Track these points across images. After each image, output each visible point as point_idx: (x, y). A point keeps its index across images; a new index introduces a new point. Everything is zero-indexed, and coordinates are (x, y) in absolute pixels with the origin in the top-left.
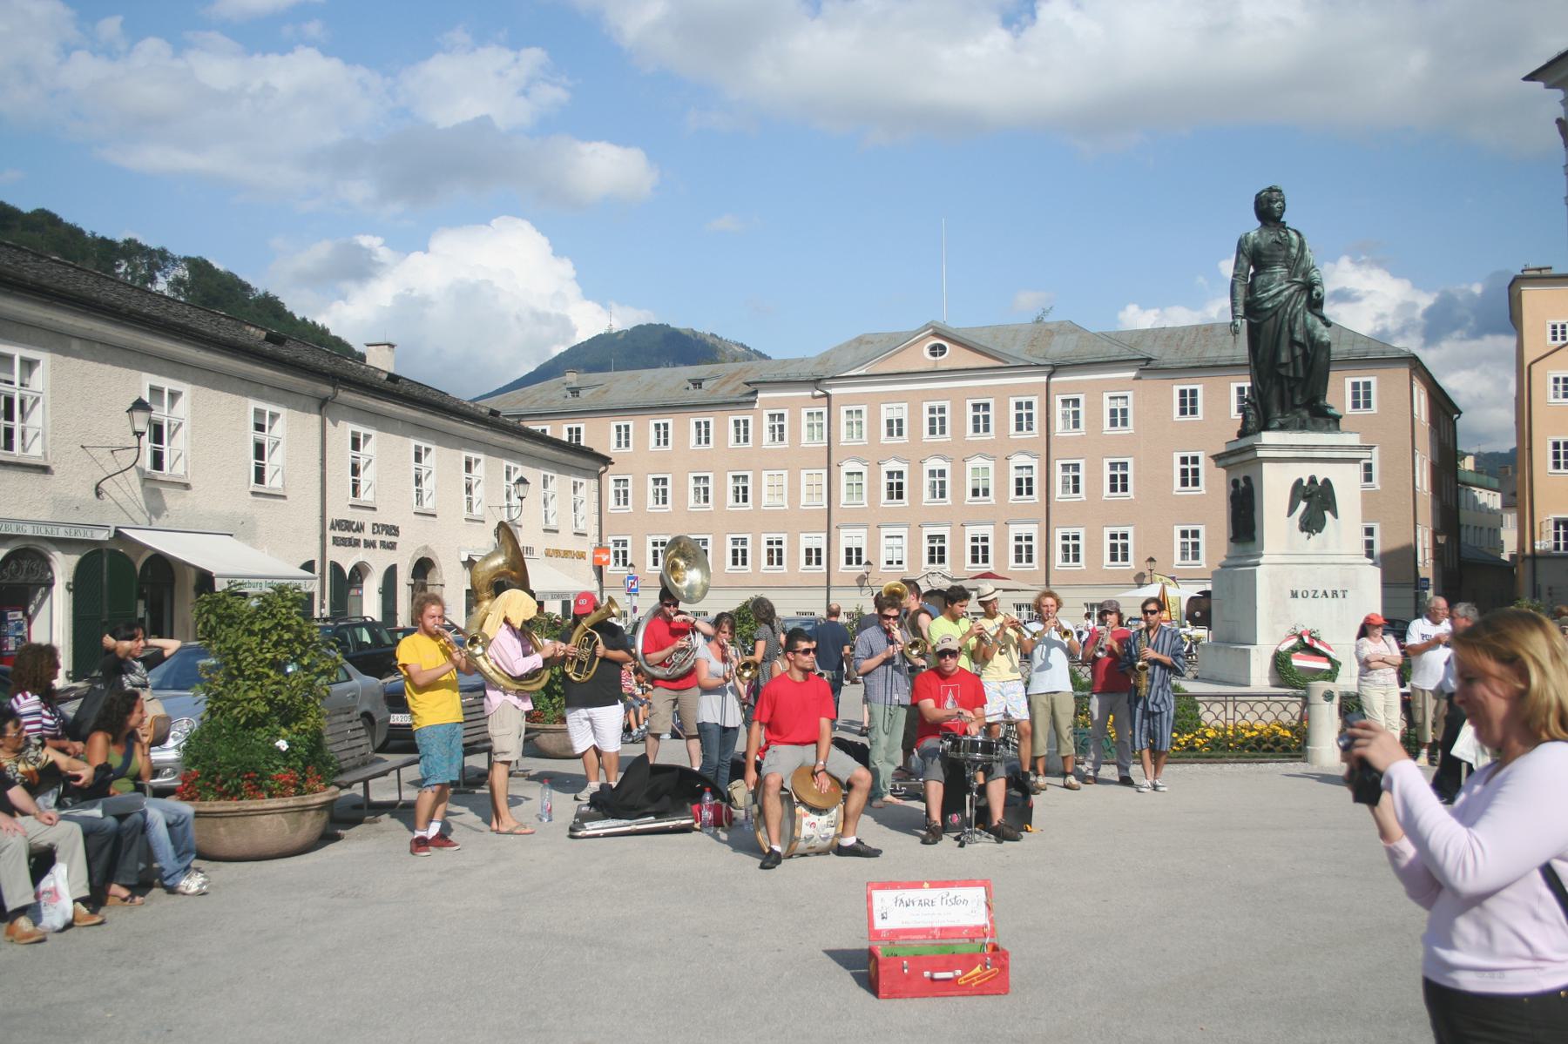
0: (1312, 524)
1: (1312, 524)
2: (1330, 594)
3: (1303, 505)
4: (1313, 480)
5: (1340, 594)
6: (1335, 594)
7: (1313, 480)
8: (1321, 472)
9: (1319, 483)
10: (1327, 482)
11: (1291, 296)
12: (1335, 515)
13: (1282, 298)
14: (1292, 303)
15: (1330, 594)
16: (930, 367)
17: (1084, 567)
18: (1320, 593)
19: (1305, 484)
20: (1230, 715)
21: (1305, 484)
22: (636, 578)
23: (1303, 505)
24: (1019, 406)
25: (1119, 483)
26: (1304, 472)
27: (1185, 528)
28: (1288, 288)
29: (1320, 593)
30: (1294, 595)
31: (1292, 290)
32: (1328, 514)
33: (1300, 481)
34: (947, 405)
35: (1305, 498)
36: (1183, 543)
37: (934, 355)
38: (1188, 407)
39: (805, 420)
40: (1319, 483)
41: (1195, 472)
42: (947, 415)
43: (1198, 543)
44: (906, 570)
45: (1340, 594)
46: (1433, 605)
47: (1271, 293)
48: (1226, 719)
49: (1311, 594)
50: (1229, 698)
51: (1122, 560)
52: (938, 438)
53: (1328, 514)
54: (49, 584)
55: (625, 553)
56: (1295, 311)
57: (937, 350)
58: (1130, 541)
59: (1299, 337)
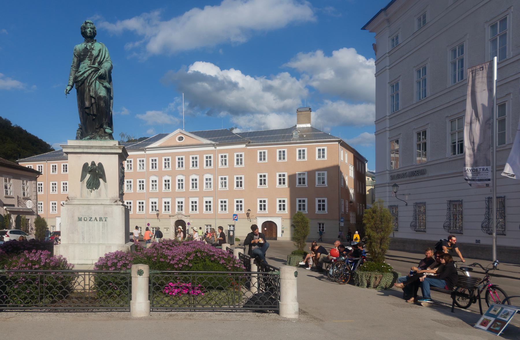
0: (93, 185)
1: (93, 185)
2: (98, 219)
3: (88, 176)
4: (93, 164)
5: (104, 220)
6: (101, 219)
7: (93, 164)
8: (98, 159)
9: (97, 165)
10: (100, 164)
11: (90, 74)
12: (105, 181)
13: (85, 75)
14: (90, 77)
15: (98, 219)
16: (177, 144)
17: (228, 213)
18: (93, 219)
19: (90, 165)
20: (87, 283)
21: (90, 165)
22: (234, 219)
23: (88, 176)
24: (207, 157)
25: (239, 184)
26: (89, 159)
27: (280, 199)
28: (88, 70)
29: (93, 219)
30: (80, 219)
31: (90, 71)
32: (101, 180)
33: (86, 165)
34: (184, 157)
35: (90, 172)
36: (319, 205)
37: (180, 140)
38: (263, 158)
39: (138, 162)
40: (97, 165)
41: (265, 180)
42: (184, 161)
43: (285, 205)
44: (171, 213)
45: (104, 220)
46: (35, 228)
47: (80, 73)
48: (85, 285)
49: (88, 219)
50: (86, 273)
51: (283, 210)
52: (181, 169)
53: (101, 180)
54: (15, 221)
55: (156, 207)
56: (91, 81)
57: (181, 139)
58: (243, 204)
59: (92, 94)
